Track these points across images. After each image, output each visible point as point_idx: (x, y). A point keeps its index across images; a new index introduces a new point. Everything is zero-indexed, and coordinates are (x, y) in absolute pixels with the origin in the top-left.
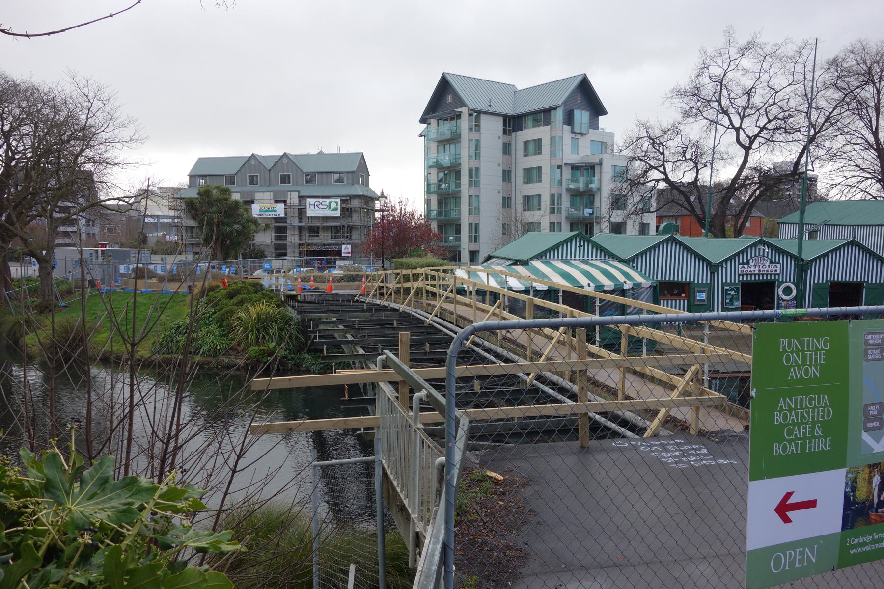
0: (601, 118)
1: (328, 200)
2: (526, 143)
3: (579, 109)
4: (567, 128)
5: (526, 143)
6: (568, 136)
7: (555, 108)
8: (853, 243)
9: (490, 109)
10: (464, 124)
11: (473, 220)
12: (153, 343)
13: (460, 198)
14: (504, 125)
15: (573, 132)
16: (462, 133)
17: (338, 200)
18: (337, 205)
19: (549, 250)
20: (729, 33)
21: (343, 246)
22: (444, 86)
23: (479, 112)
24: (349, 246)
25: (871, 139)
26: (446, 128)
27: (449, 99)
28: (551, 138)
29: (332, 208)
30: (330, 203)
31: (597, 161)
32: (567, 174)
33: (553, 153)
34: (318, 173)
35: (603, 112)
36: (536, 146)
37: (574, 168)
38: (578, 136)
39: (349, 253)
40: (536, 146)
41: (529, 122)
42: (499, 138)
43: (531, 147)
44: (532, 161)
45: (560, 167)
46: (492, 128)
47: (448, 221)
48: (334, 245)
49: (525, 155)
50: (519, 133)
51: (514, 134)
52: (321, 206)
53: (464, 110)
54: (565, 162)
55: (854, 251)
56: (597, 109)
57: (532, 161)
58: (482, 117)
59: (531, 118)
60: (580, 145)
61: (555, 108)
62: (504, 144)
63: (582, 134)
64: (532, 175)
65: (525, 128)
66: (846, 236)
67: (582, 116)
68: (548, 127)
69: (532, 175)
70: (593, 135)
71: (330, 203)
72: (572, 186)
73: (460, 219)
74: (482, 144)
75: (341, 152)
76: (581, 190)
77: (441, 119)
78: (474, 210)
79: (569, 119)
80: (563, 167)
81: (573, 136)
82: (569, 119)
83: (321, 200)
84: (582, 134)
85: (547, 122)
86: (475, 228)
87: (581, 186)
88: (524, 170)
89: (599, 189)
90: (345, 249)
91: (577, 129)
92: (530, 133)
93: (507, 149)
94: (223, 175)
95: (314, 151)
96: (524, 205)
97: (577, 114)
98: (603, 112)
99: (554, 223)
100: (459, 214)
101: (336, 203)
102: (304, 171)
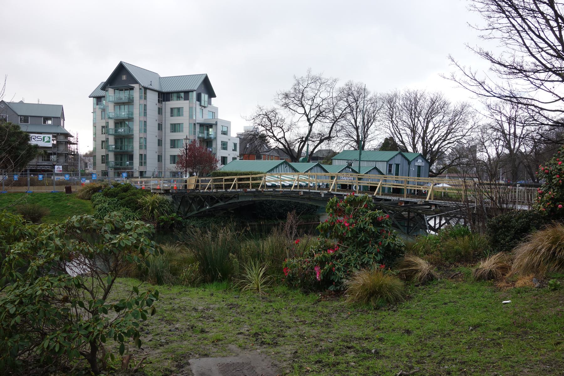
0: (212, 99)
1: (42, 136)
2: (172, 109)
3: (204, 93)
4: (198, 103)
5: (172, 109)
6: (198, 107)
7: (192, 91)
8: (375, 168)
9: (150, 87)
10: (136, 94)
11: (142, 152)
12: (344, 187)
13: (133, 138)
14: (159, 97)
15: (201, 105)
16: (135, 99)
17: (51, 136)
18: (50, 139)
19: (275, 168)
20: (309, 71)
21: (56, 167)
22: (121, 69)
23: (146, 89)
24: (61, 167)
25: (354, 123)
26: (124, 96)
27: (124, 77)
28: (189, 107)
29: (45, 141)
30: (44, 137)
31: (214, 123)
32: (198, 128)
33: (191, 116)
34: (30, 116)
35: (214, 96)
36: (177, 111)
37: (201, 125)
38: (203, 108)
39: (61, 171)
40: (177, 111)
41: (175, 96)
42: (156, 104)
43: (175, 112)
44: (176, 120)
45: (195, 124)
46: (152, 98)
47: (124, 152)
48: (46, 165)
49: (172, 116)
50: (167, 103)
51: (164, 103)
52: (36, 139)
53: (136, 86)
54: (197, 122)
55: (375, 171)
56: (211, 94)
57: (176, 120)
58: (148, 91)
59: (175, 95)
60: (204, 112)
61: (192, 91)
62: (159, 108)
63: (205, 107)
64: (175, 128)
65: (172, 100)
66: (373, 165)
67: (205, 97)
68: (187, 101)
69: (175, 128)
70: (209, 108)
71: (44, 137)
72: (200, 136)
73: (133, 151)
74: (148, 107)
75: (40, 103)
76: (205, 138)
77: (118, 89)
78: (143, 146)
79: (199, 98)
80: (196, 124)
81: (200, 107)
82: (199, 98)
83: (37, 135)
84: (205, 107)
85: (187, 98)
86: (143, 158)
87: (205, 136)
88: (171, 124)
89: (215, 138)
90: (57, 168)
91: (203, 104)
92: (174, 103)
93: (160, 111)
94: (41, 117)
95: (17, 100)
96: (171, 145)
97: (203, 95)
98: (214, 96)
99: (142, 155)
100: (133, 148)
101: (49, 138)
102: (19, 114)
